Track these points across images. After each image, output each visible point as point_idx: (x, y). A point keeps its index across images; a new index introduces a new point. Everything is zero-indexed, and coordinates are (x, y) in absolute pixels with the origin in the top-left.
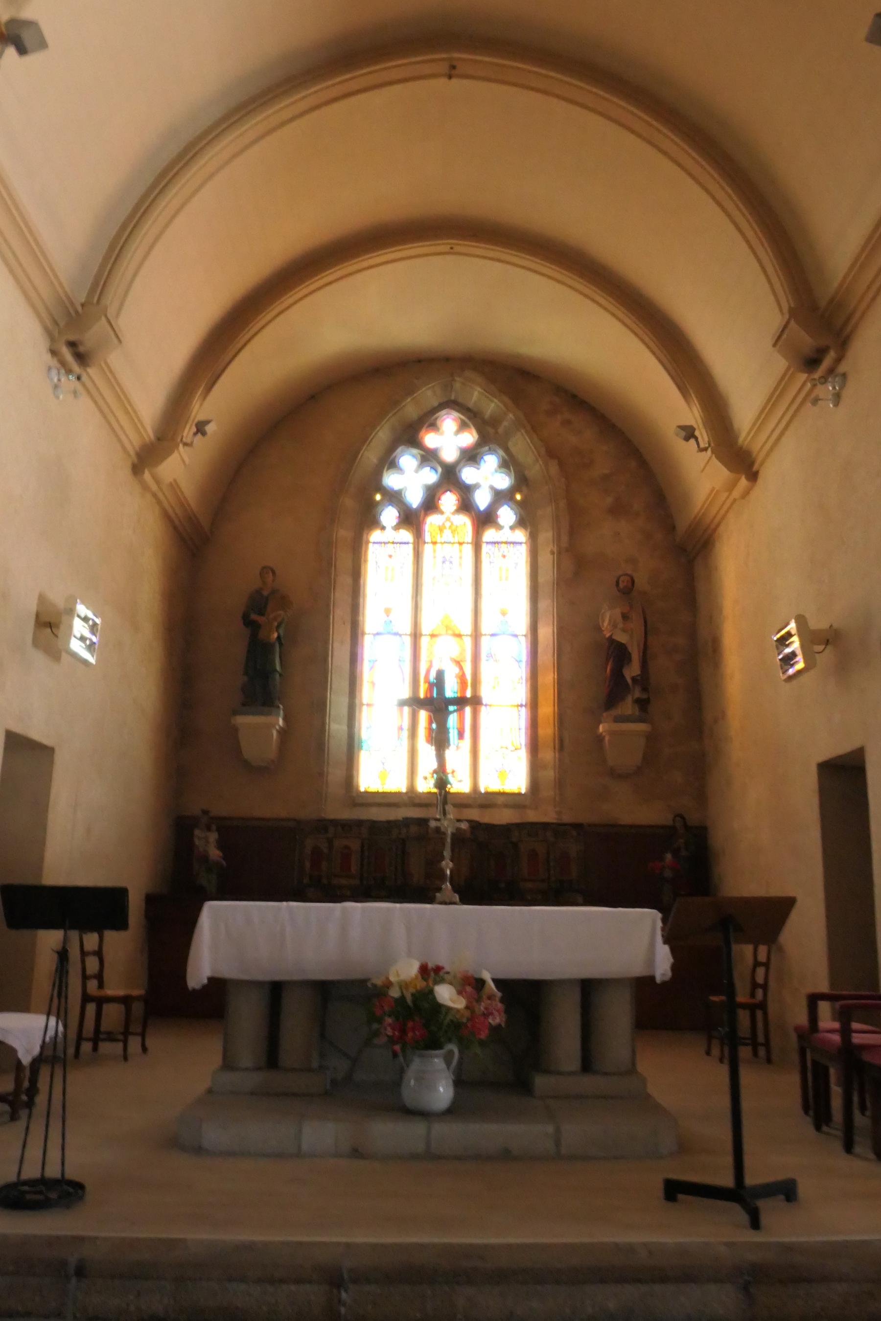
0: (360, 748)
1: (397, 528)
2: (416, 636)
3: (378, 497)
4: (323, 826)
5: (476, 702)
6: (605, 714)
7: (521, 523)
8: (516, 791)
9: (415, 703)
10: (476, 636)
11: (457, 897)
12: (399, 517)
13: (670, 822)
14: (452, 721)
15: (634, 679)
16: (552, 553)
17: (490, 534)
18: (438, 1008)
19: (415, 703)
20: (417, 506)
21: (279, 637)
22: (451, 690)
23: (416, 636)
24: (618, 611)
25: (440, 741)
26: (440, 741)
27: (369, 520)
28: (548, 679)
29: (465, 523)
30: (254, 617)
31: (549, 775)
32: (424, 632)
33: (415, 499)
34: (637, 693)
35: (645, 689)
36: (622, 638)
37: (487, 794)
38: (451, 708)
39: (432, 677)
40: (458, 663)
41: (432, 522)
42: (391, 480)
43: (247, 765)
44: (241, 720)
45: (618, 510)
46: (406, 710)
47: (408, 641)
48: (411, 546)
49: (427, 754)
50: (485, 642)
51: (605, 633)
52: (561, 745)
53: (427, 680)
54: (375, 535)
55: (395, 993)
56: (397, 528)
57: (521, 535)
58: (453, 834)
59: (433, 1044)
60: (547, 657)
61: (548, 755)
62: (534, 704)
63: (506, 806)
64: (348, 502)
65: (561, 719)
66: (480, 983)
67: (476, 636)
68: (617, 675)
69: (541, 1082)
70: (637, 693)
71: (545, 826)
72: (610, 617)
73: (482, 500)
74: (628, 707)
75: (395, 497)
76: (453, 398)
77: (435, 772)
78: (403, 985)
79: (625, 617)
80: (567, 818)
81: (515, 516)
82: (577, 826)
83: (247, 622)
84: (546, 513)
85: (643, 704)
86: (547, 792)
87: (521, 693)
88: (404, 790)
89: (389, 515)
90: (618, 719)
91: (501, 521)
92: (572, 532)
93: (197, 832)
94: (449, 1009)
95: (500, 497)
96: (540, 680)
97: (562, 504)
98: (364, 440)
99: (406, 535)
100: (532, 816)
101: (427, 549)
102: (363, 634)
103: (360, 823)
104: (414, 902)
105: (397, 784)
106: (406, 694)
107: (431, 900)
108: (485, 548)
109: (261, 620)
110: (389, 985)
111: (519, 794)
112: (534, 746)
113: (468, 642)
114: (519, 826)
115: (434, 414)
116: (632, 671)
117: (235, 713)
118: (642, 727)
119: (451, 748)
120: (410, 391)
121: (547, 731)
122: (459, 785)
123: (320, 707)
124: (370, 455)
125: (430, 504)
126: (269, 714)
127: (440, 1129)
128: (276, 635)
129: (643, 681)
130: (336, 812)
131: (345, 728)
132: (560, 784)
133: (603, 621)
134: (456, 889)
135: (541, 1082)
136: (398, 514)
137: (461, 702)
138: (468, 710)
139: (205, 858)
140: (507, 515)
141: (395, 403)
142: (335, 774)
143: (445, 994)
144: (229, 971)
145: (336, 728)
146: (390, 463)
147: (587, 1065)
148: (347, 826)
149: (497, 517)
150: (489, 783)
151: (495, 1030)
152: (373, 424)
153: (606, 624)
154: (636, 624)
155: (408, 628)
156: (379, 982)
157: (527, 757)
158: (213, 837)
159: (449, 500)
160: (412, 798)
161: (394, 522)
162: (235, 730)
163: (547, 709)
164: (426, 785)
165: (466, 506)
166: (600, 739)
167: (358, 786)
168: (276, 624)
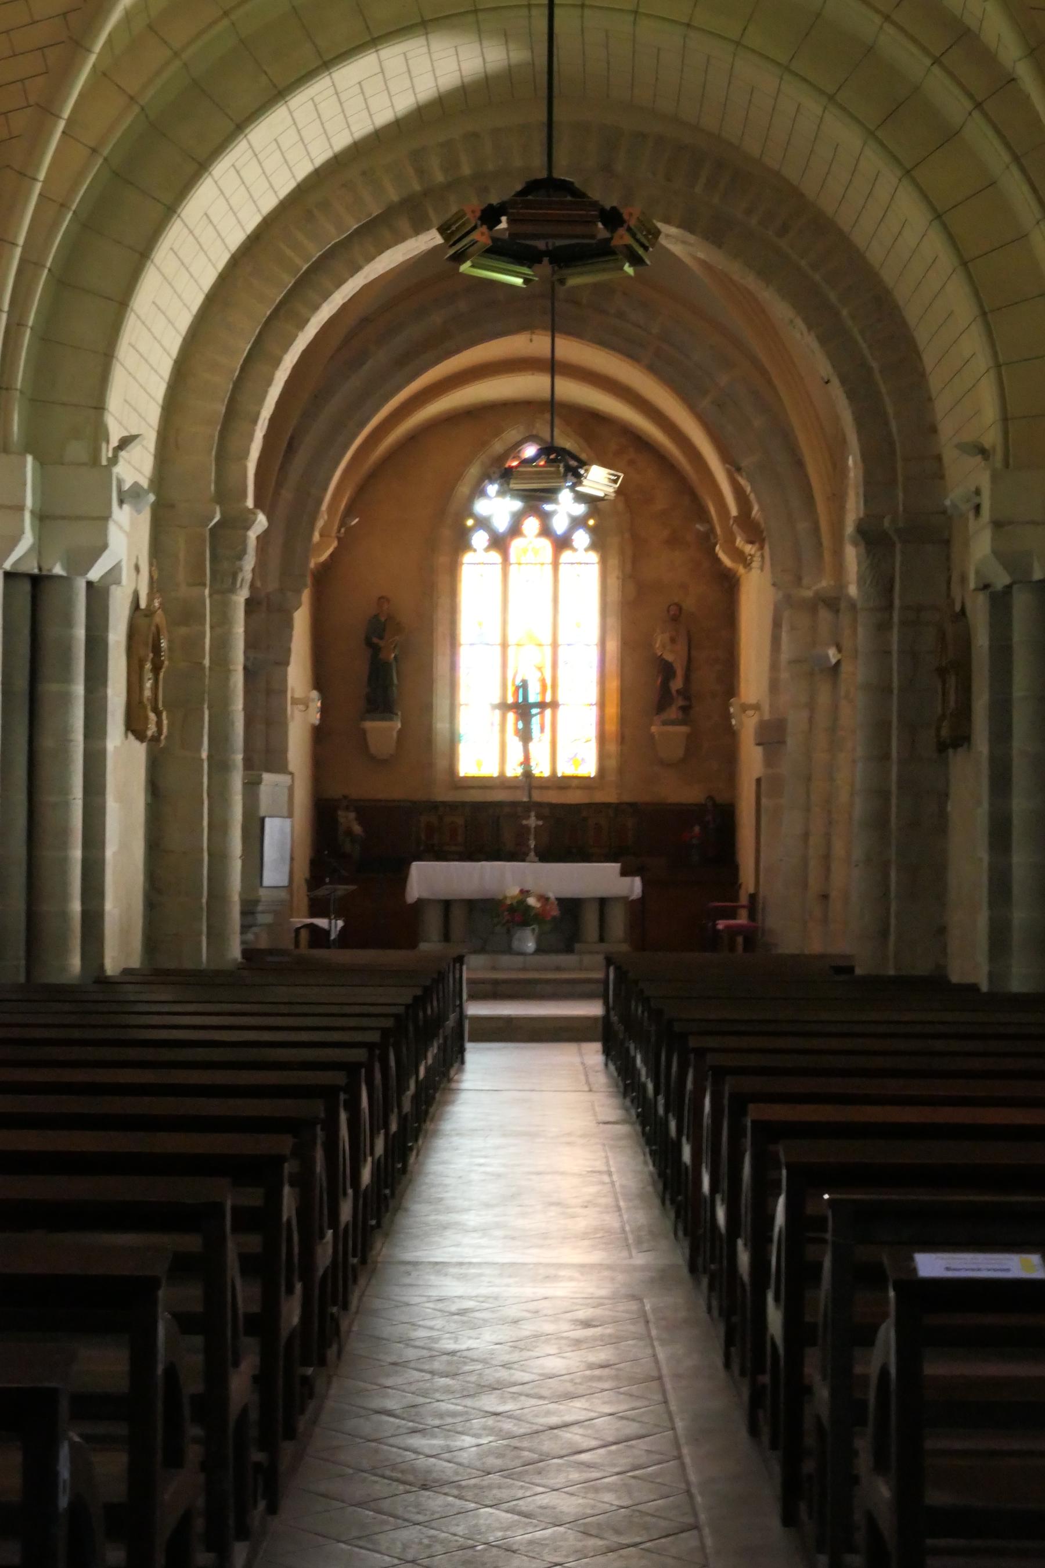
0: (459, 741)
1: (487, 549)
2: (504, 646)
3: (470, 522)
4: (434, 806)
5: (554, 705)
6: (655, 718)
7: (594, 546)
8: (586, 775)
9: (504, 707)
10: (555, 645)
11: (537, 859)
12: (489, 540)
13: (703, 802)
14: (535, 722)
15: (678, 691)
16: (618, 578)
17: (566, 556)
18: (529, 908)
19: (504, 707)
20: (504, 531)
21: (395, 657)
22: (533, 697)
23: (504, 646)
24: (666, 636)
25: (525, 736)
26: (525, 736)
27: (461, 542)
28: (614, 684)
29: (546, 546)
30: (375, 640)
31: (612, 763)
32: (510, 643)
33: (501, 524)
34: (681, 702)
35: (687, 698)
36: (669, 657)
37: (564, 778)
38: (534, 711)
39: (518, 682)
40: (540, 669)
41: (516, 546)
42: (481, 507)
43: (372, 758)
44: (368, 725)
45: (673, 541)
46: (498, 713)
47: (498, 650)
48: (500, 566)
49: (515, 746)
50: (561, 651)
51: (658, 651)
52: (622, 739)
53: (514, 684)
54: (467, 558)
55: (508, 902)
56: (487, 549)
57: (594, 557)
58: (535, 828)
59: (525, 923)
60: (613, 666)
61: (612, 748)
62: (602, 705)
63: (578, 788)
64: (446, 533)
65: (623, 720)
66: (547, 899)
67: (555, 645)
68: (665, 687)
69: (577, 946)
70: (681, 702)
71: (607, 805)
72: (661, 641)
73: (560, 525)
74: (673, 713)
75: (483, 523)
76: (534, 432)
77: (521, 764)
78: (512, 898)
79: (673, 640)
80: (627, 798)
81: (589, 539)
82: (633, 806)
83: (369, 643)
84: (614, 541)
85: (685, 709)
86: (612, 777)
87: (592, 694)
88: (496, 774)
89: (480, 539)
90: (665, 723)
91: (575, 544)
92: (635, 561)
93: (340, 813)
94: (534, 908)
95: (577, 523)
96: (607, 685)
97: (627, 535)
98: (459, 477)
99: (495, 556)
100: (600, 797)
101: (513, 570)
102: (460, 645)
103: (464, 804)
104: (607, 862)
105: (489, 769)
106: (497, 700)
107: (523, 860)
108: (561, 567)
109: (382, 643)
110: (505, 898)
111: (589, 778)
112: (602, 739)
113: (548, 651)
114: (589, 805)
115: (516, 449)
116: (677, 684)
117: (363, 719)
118: (684, 729)
119: (534, 740)
120: (497, 433)
121: (612, 727)
122: (541, 769)
123: (427, 708)
124: (464, 489)
125: (515, 530)
126: (391, 719)
127: (528, 958)
128: (393, 655)
129: (685, 693)
130: (443, 795)
131: (447, 725)
132: (621, 771)
133: (656, 643)
134: (537, 854)
135: (577, 946)
136: (488, 538)
137: (542, 705)
138: (548, 712)
139: (349, 832)
140: (581, 538)
141: (484, 444)
142: (441, 763)
143: (531, 901)
144: (425, 895)
145: (441, 726)
146: (480, 492)
147: (602, 939)
148: (453, 807)
149: (572, 540)
150: (565, 769)
151: (554, 918)
152: (466, 463)
153: (657, 645)
154: (682, 646)
155: (498, 640)
156: (500, 897)
157: (597, 747)
158: (352, 815)
159: (531, 525)
160: (502, 783)
161: (486, 544)
162: (364, 732)
163: (613, 710)
164: (514, 770)
165: (546, 531)
166: (652, 736)
167: (458, 773)
168: (393, 646)
